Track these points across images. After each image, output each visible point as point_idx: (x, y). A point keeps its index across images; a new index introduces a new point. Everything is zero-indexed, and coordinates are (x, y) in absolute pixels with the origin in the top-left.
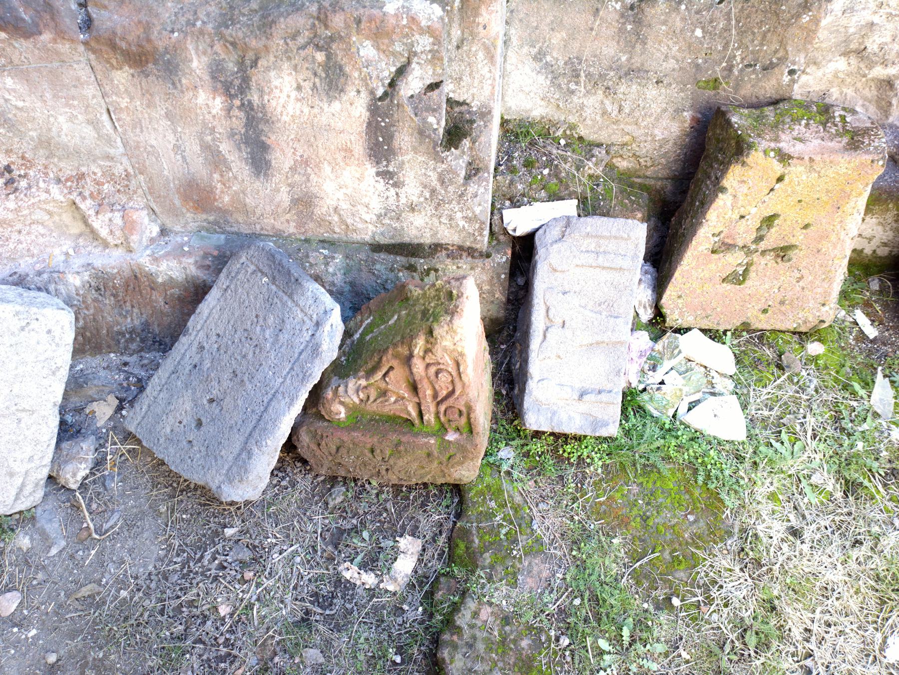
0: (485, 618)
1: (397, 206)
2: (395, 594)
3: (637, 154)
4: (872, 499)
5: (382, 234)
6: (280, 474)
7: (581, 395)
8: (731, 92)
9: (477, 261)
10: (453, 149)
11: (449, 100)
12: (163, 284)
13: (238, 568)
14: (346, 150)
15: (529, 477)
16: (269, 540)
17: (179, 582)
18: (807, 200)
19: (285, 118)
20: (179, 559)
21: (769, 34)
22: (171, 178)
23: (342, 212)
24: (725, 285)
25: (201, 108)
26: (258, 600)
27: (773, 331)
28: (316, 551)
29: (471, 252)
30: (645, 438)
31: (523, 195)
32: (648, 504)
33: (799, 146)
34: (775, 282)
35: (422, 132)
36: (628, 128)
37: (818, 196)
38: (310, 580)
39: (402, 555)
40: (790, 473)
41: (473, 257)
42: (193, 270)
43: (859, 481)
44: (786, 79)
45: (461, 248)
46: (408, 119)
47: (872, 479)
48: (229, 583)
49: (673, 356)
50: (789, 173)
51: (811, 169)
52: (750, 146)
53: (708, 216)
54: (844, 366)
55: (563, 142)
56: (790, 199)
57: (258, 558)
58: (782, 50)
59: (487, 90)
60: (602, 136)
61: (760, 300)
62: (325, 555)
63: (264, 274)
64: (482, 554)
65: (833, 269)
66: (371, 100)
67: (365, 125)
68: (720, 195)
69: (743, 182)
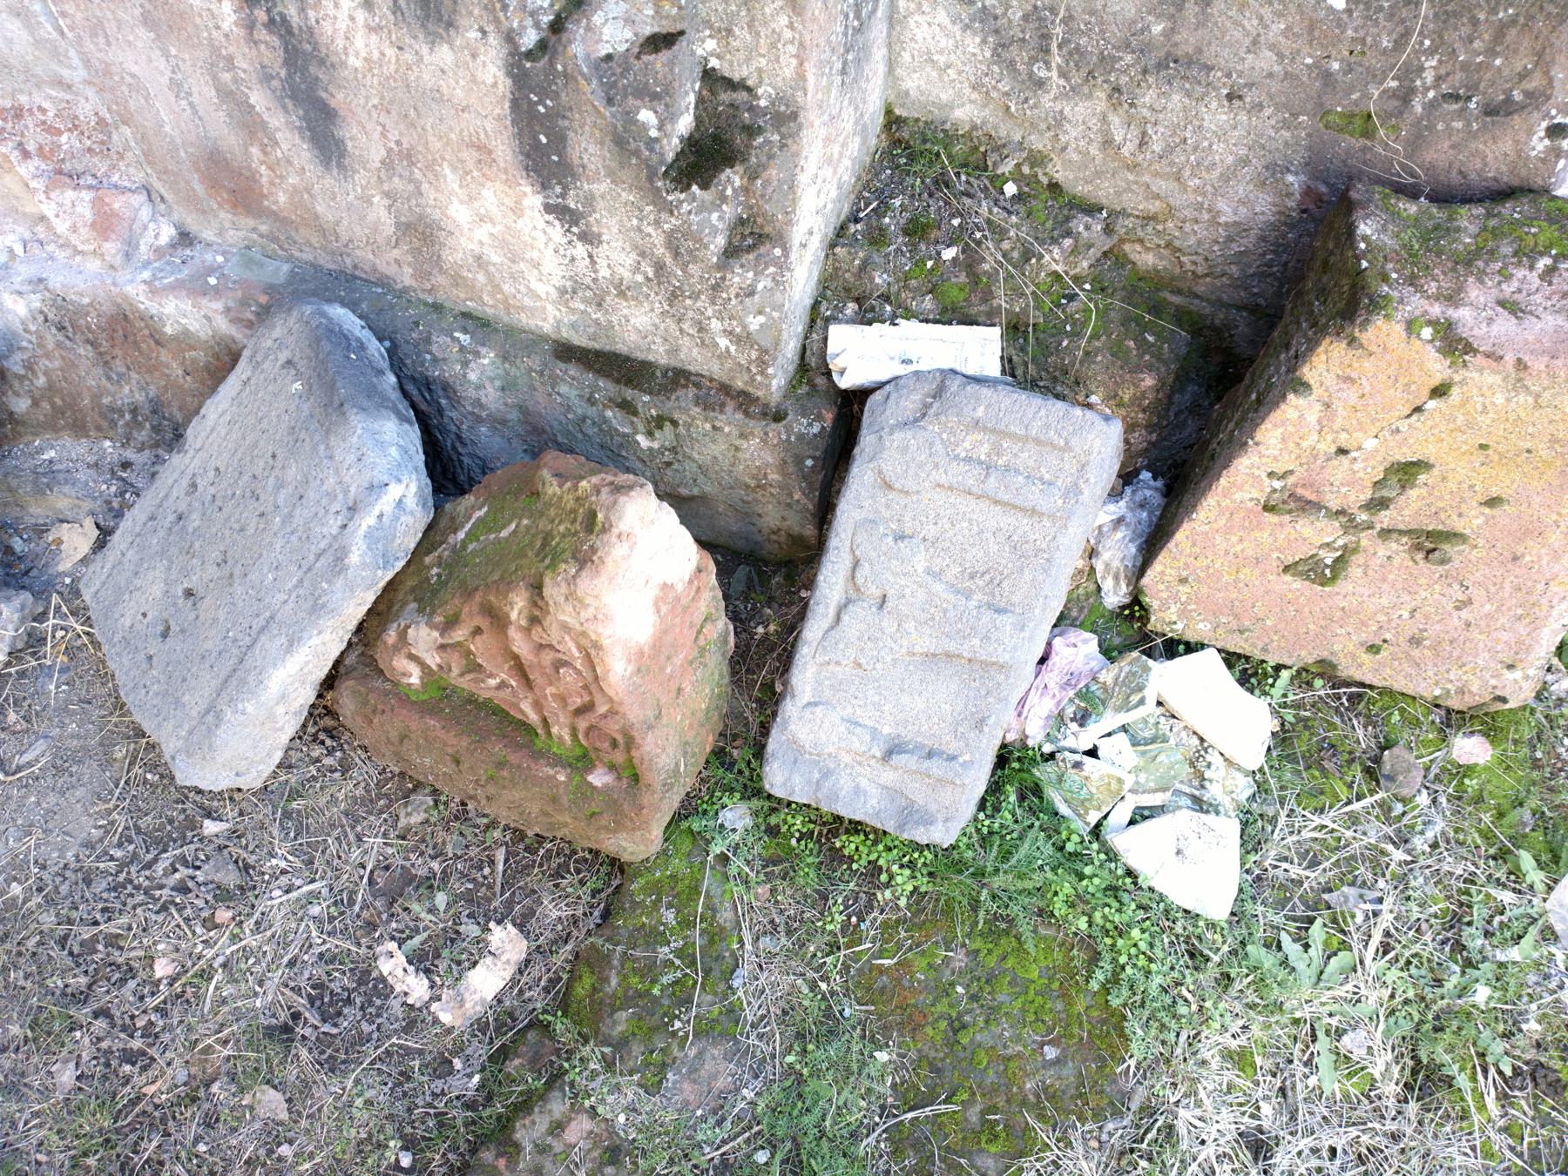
0: (573, 1140)
1: (595, 280)
2: (450, 1031)
3: (1177, 243)
4: (1462, 1118)
5: (573, 326)
6: (328, 742)
7: (889, 754)
8: (1396, 152)
9: (752, 423)
10: (695, 188)
11: (709, 76)
12: (175, 338)
13: (209, 898)
14: (479, 148)
15: (762, 877)
16: (274, 862)
17: (105, 895)
18: (1501, 448)
19: (353, 61)
20: (118, 853)
21: (1513, 32)
22: (179, 141)
23: (492, 269)
24: (1288, 578)
25: (200, 15)
26: (224, 965)
27: (1387, 692)
28: (352, 903)
29: (745, 401)
30: (1013, 861)
31: (886, 298)
32: (974, 998)
33: (1505, 325)
34: (1406, 597)
35: (624, 140)
36: (1160, 186)
37: (1528, 445)
38: (321, 955)
39: (489, 960)
40: (1298, 1015)
41: (746, 413)
42: (223, 325)
43: (1445, 1071)
44: (1539, 144)
45: (725, 389)
46: (589, 108)
47: (1480, 1077)
48: (187, 920)
49: (1126, 707)
50: (1463, 382)
51: (1519, 385)
52: (1378, 305)
53: (1259, 436)
54: (1521, 805)
55: (1010, 189)
56: (1460, 437)
57: (243, 891)
58: (1538, 75)
59: (788, 69)
60: (1103, 191)
61: (1364, 624)
62: (365, 914)
63: (298, 376)
64: (614, 1010)
65: (1544, 601)
66: (511, 54)
67: (507, 105)
68: (1291, 397)
69: (1348, 379)
